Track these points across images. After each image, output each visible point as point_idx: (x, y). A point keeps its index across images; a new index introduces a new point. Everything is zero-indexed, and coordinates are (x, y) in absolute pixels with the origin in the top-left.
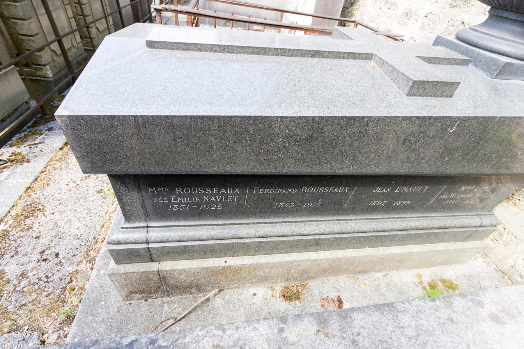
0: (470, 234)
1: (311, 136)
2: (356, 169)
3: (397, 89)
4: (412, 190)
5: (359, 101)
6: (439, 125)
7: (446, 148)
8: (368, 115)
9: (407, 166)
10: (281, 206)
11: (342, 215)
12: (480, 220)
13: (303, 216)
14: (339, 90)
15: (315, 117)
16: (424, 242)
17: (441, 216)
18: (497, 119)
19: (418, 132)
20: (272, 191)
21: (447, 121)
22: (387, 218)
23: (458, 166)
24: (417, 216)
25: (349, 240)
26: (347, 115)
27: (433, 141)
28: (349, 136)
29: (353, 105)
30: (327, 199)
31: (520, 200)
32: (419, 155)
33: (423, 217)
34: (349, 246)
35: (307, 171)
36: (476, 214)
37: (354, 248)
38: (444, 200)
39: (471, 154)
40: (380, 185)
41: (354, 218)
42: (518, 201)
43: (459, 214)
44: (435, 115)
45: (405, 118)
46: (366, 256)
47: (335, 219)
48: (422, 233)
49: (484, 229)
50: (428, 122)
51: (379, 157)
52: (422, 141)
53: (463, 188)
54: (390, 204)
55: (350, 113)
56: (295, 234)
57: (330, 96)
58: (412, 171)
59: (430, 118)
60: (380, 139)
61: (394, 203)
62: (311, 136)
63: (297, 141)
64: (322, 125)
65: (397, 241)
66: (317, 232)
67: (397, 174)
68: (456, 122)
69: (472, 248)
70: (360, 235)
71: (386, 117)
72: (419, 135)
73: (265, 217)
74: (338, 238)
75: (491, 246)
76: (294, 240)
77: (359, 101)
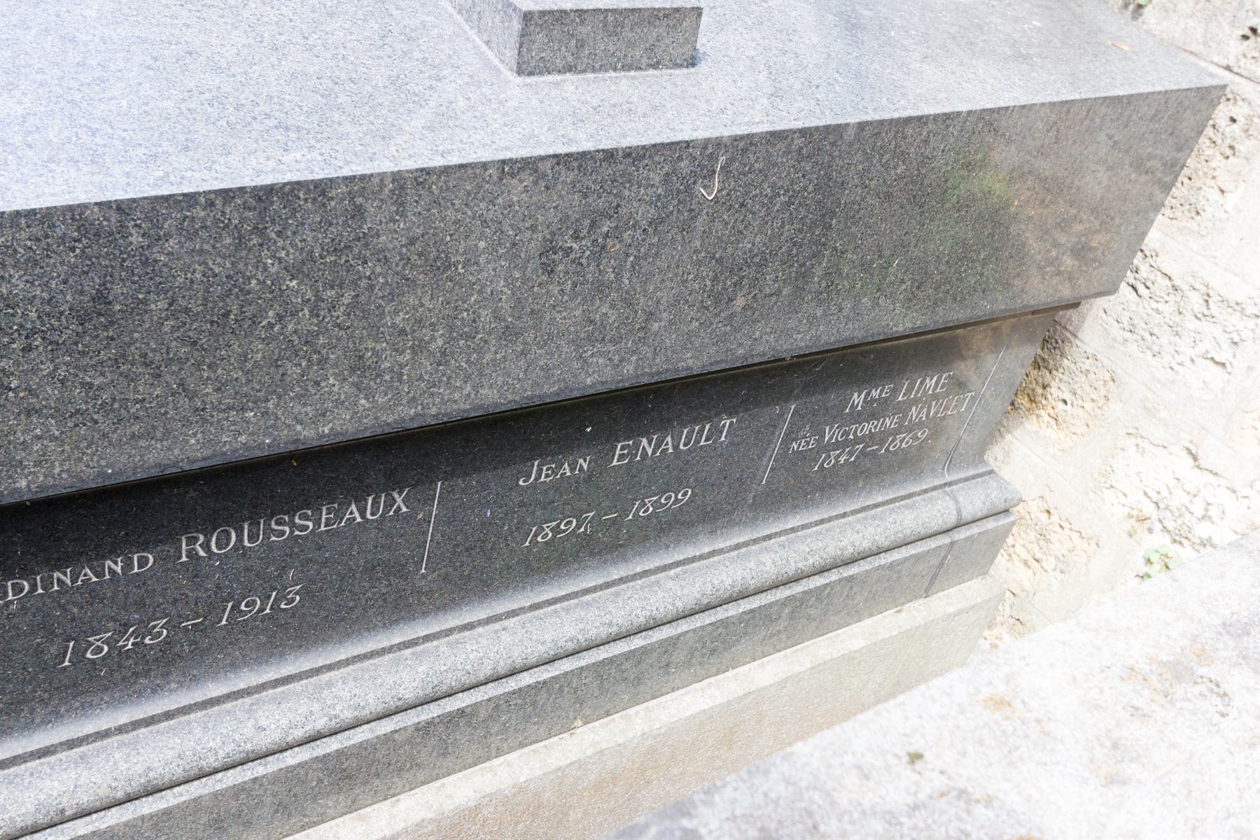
0: (935, 561)
1: (101, 297)
2: (388, 408)
3: (484, 48)
4: (676, 447)
5: (309, 114)
6: (656, 178)
7: (720, 261)
8: (346, 172)
9: (600, 354)
10: (98, 647)
11: (425, 614)
12: (952, 505)
13: (234, 666)
14: (217, 69)
15: (84, 207)
16: (793, 637)
17: (822, 522)
18: (850, 134)
19: (584, 216)
20: (18, 589)
21: (681, 163)
22: (622, 580)
23: (792, 323)
24: (735, 541)
25: (483, 714)
26: (248, 181)
27: (661, 244)
28: (294, 271)
29: (279, 135)
30: (325, 564)
31: (1065, 402)
32: (629, 303)
33: (755, 541)
34: (495, 741)
35: (151, 458)
36: (937, 482)
37: (522, 745)
38: (802, 456)
39: (819, 271)
40: (538, 450)
41: (483, 615)
42: (1061, 406)
43: (880, 499)
44: (625, 143)
45: (510, 168)
46: (580, 764)
47: (397, 640)
48: (771, 605)
49: (975, 530)
50: (607, 171)
51: (469, 337)
52: (615, 246)
53: (858, 399)
54: (614, 521)
55: (259, 173)
56: (211, 762)
57: (169, 104)
58: (629, 369)
59: (610, 155)
60: (440, 265)
61: (626, 512)
62: (101, 297)
63: (34, 331)
64: (136, 239)
65: (688, 664)
66: (321, 724)
67: (576, 394)
68: (712, 158)
69: (959, 613)
70: (526, 679)
71: (427, 171)
72: (593, 225)
73: (30, 726)
74: (430, 723)
75: (1027, 585)
76: (215, 795)
77: (309, 114)
